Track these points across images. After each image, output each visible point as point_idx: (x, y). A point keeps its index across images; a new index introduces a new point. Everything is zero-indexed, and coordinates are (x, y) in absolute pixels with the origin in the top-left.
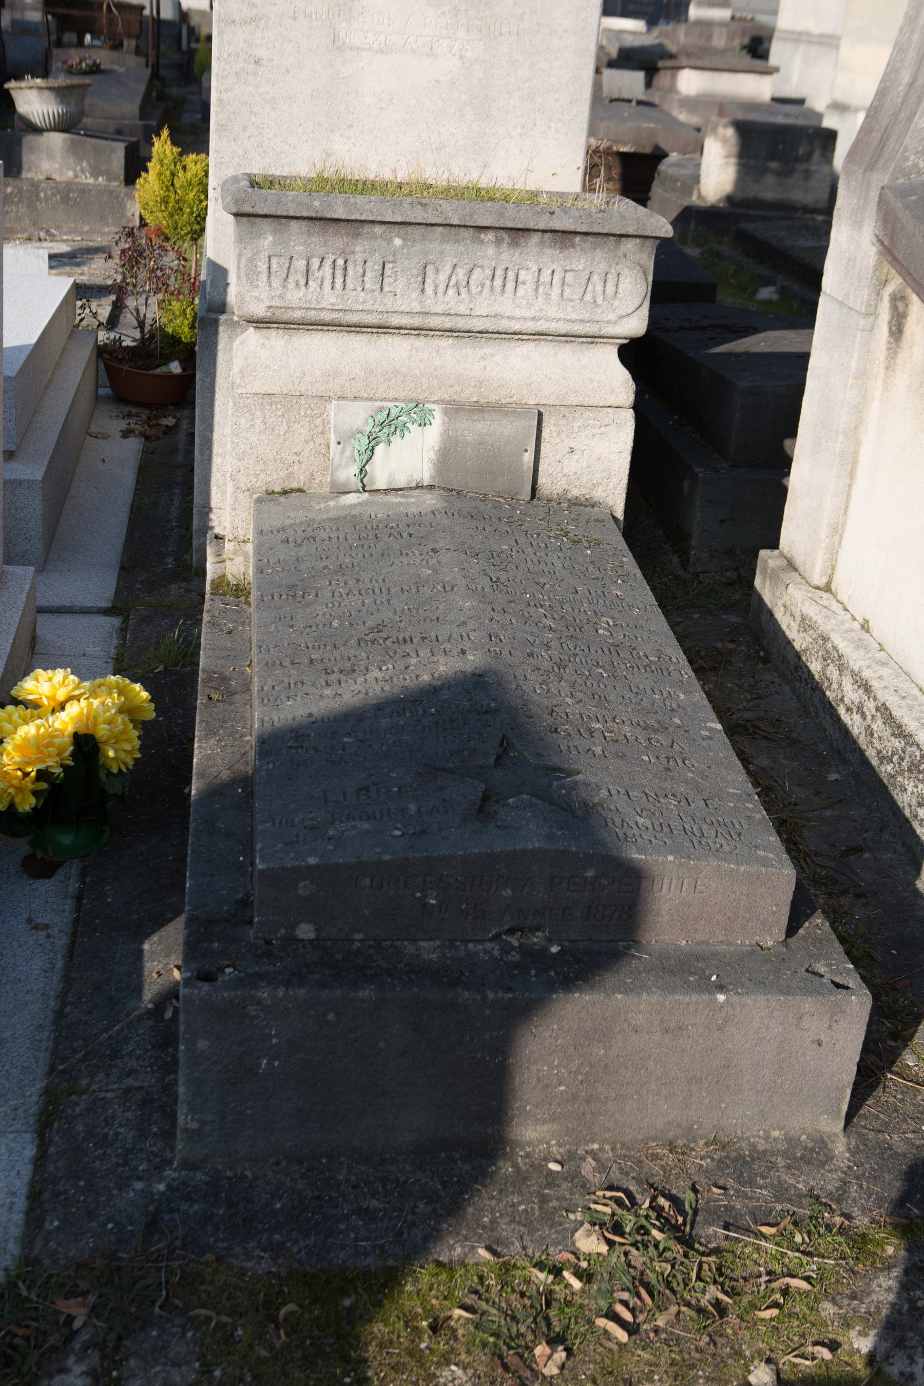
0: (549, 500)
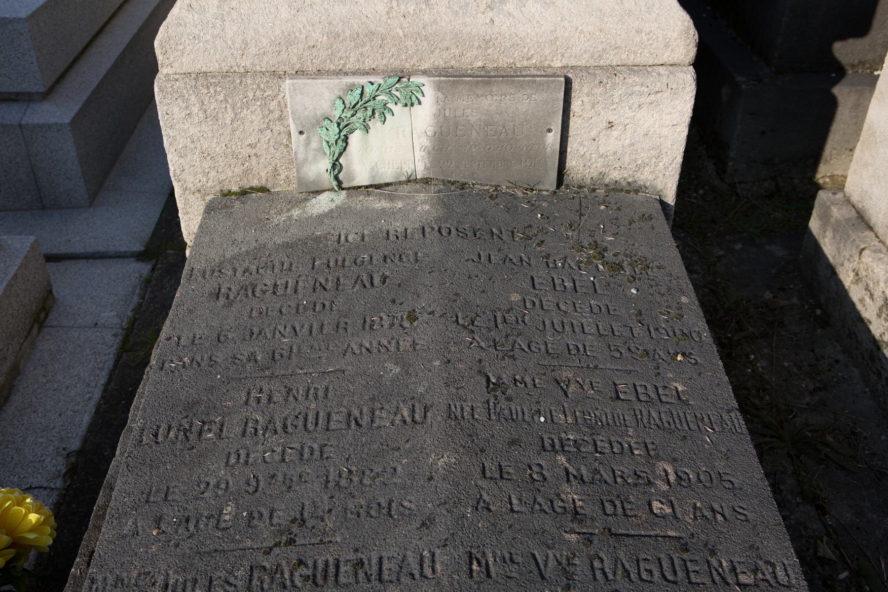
0: (580, 187)
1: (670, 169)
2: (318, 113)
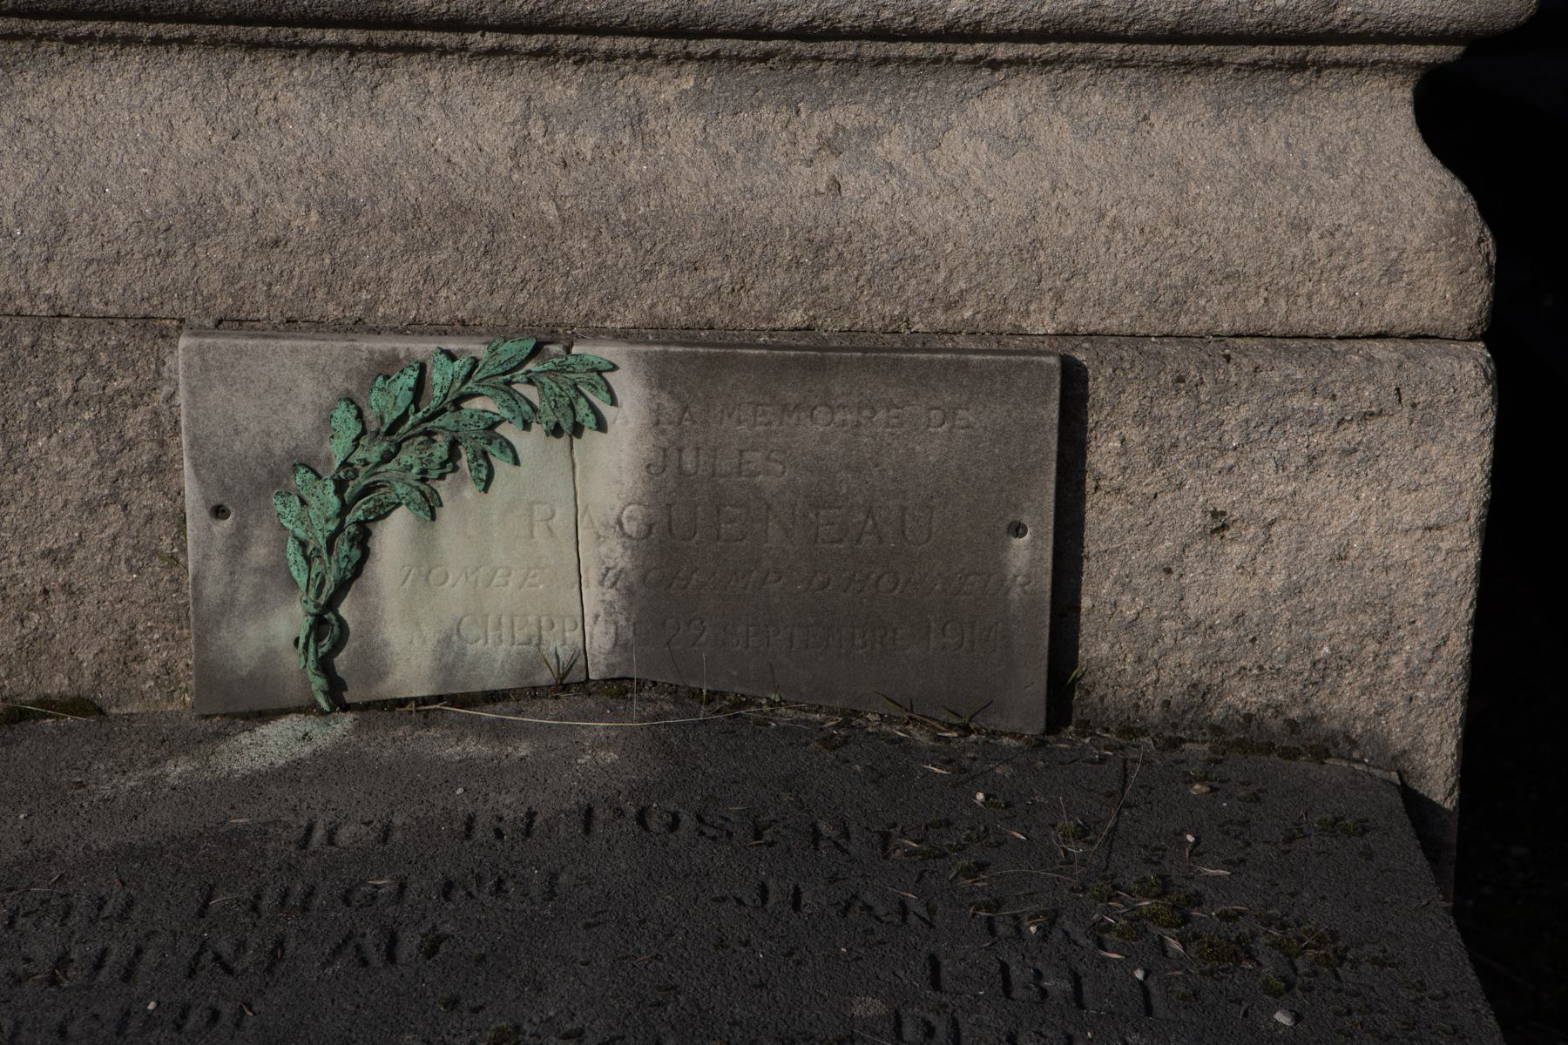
0: (1128, 731)
1: (1430, 678)
2: (278, 448)
